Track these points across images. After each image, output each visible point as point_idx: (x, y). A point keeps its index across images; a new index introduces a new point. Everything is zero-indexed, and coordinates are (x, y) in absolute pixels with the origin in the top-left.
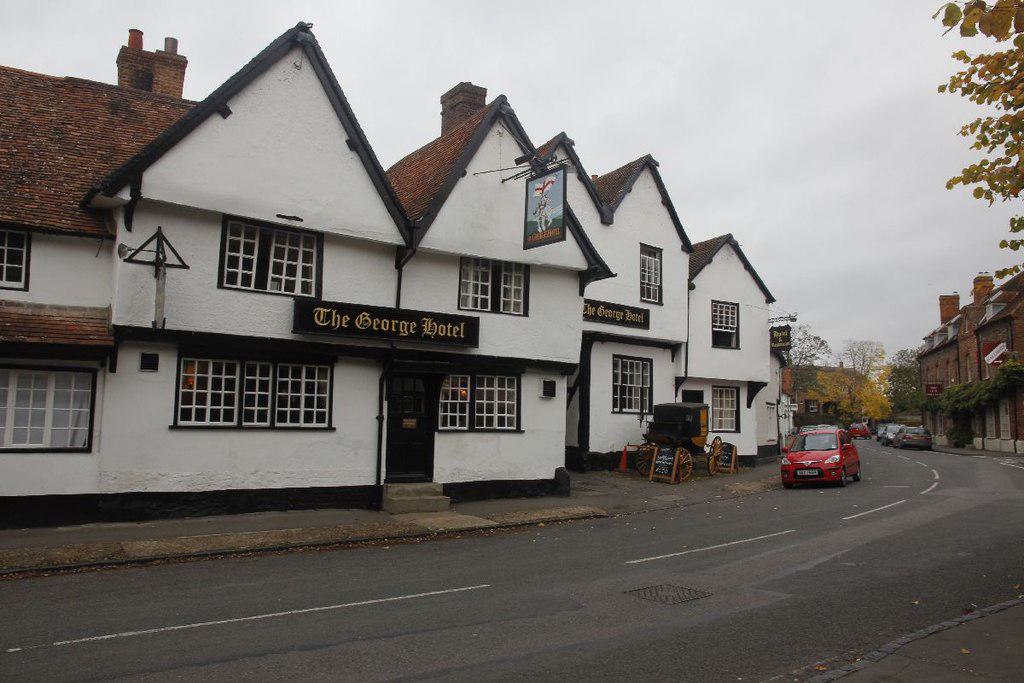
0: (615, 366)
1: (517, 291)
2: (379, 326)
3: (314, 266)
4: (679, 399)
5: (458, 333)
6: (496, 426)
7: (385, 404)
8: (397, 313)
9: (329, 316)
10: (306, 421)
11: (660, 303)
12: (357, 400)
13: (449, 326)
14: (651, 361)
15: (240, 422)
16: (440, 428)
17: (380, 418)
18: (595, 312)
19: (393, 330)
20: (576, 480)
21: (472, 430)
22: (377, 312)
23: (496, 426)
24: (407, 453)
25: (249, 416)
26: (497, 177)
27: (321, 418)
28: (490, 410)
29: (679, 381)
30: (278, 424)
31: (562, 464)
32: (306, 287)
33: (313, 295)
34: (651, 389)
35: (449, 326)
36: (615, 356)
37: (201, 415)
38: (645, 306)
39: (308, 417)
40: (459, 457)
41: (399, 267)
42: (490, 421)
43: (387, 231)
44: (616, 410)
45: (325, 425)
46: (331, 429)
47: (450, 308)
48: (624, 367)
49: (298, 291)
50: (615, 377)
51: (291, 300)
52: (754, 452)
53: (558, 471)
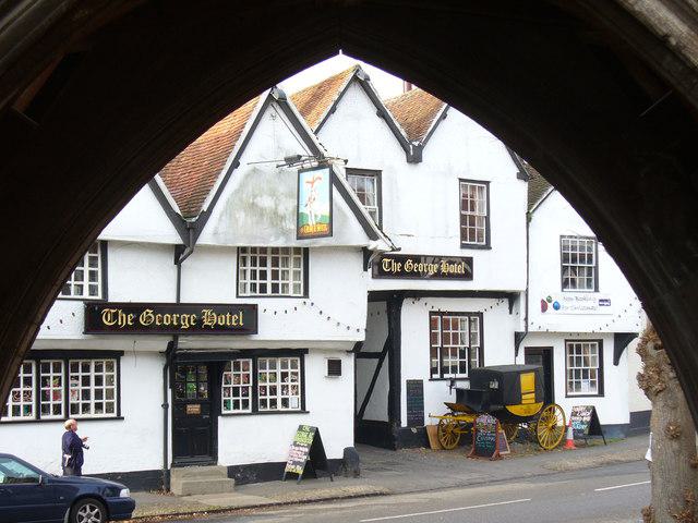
0: (433, 324)
1: (297, 274)
2: (161, 320)
3: (99, 269)
4: (521, 360)
5: (238, 321)
6: (279, 407)
7: (169, 392)
8: (178, 308)
9: (115, 316)
10: (243, 408)
11: (488, 247)
12: (143, 387)
13: (228, 315)
14: (480, 315)
15: (38, 416)
16: (224, 412)
17: (165, 406)
18: (402, 268)
19: (175, 323)
20: (370, 457)
21: (255, 412)
22: (158, 308)
23: (279, 407)
24: (192, 436)
25: (45, 409)
26: (275, 164)
27: (110, 409)
28: (273, 391)
29: (518, 337)
30: (43, 417)
31: (350, 443)
32: (93, 290)
33: (100, 297)
34: (481, 349)
35: (228, 315)
36: (431, 313)
37: (86, 408)
38: (467, 253)
39: (99, 407)
40: (245, 438)
41: (178, 262)
42: (274, 402)
43: (174, 238)
44: (435, 376)
45: (114, 415)
46: (119, 418)
47: (228, 296)
48: (445, 325)
49: (86, 295)
50: (433, 338)
51: (81, 304)
52: (626, 420)
53: (347, 451)
